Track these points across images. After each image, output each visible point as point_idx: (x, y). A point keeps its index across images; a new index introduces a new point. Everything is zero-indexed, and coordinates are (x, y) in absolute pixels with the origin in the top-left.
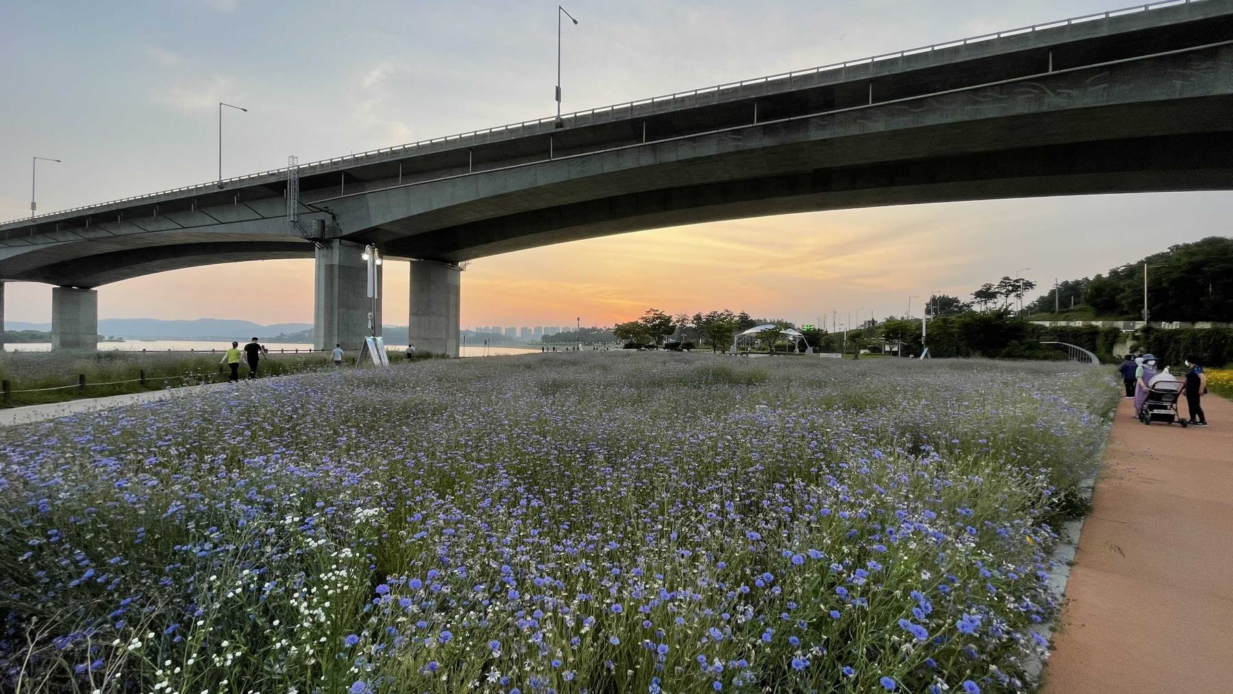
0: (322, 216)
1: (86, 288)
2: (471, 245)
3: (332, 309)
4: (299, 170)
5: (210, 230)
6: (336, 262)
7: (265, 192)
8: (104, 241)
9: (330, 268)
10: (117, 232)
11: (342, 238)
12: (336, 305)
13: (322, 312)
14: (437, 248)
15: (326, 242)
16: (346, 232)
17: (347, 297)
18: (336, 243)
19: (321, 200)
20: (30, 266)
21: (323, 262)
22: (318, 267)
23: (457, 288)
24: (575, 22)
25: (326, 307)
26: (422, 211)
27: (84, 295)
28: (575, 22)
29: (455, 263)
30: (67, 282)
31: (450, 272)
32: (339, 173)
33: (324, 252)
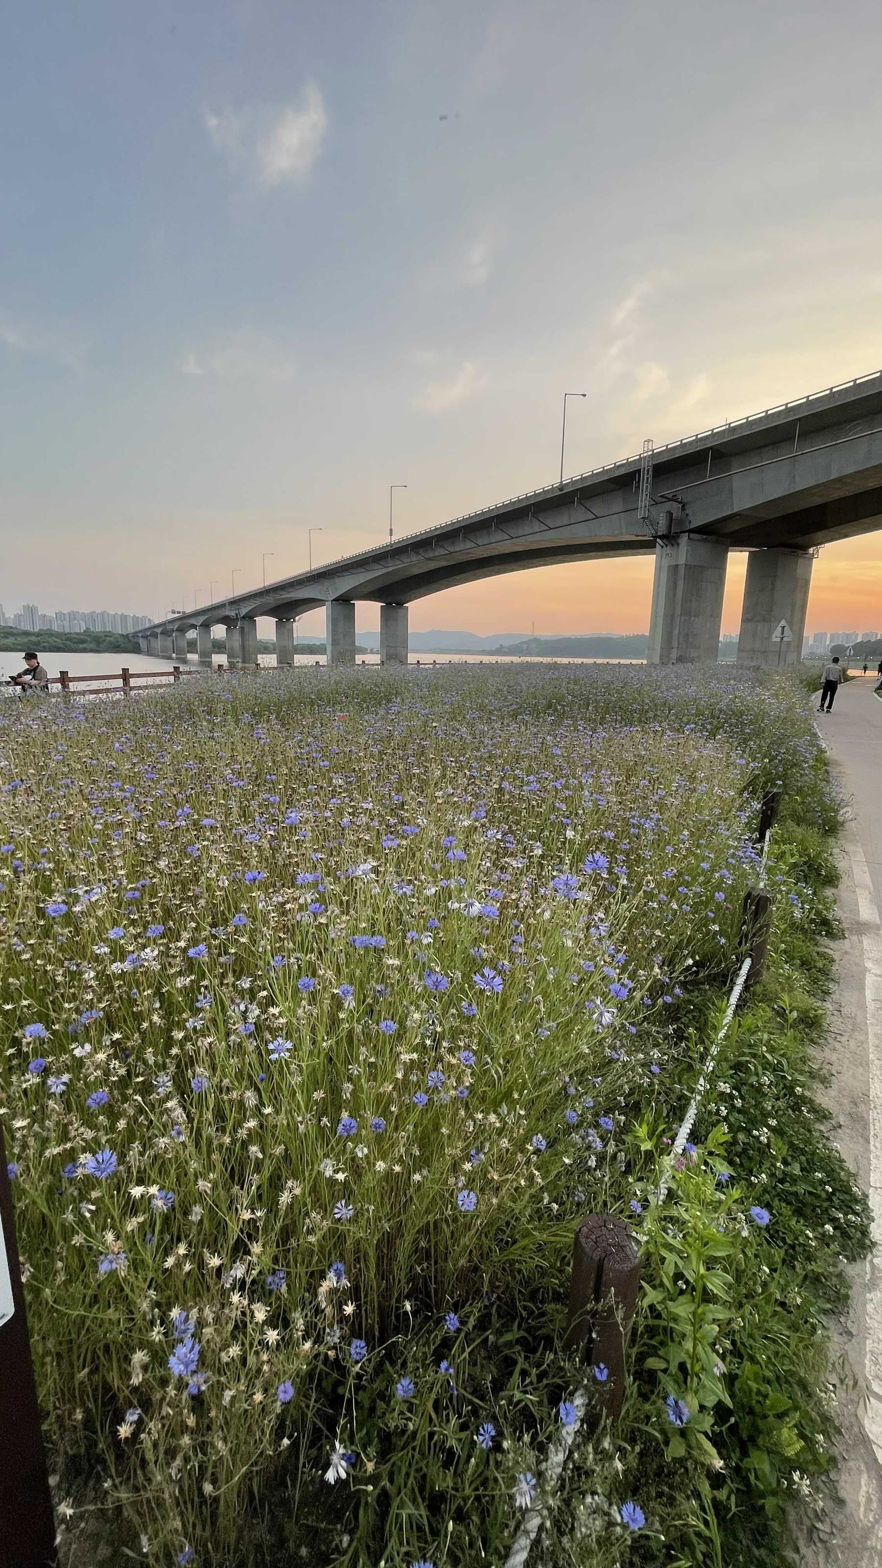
0: (668, 506)
1: (400, 604)
2: (499, 564)
3: (672, 617)
4: (654, 456)
5: (537, 537)
6: (682, 561)
7: (620, 483)
8: (416, 564)
9: (674, 569)
10: (451, 549)
11: (691, 531)
12: (678, 611)
13: (660, 621)
14: (786, 535)
15: (670, 538)
16: (698, 521)
17: (688, 598)
18: (684, 539)
19: (678, 488)
20: (371, 588)
21: (666, 563)
22: (659, 569)
23: (807, 582)
24: (584, 395)
25: (665, 615)
26: (812, 483)
27: (401, 612)
28: (584, 395)
29: (806, 548)
30: (389, 601)
31: (801, 561)
32: (706, 451)
33: (669, 550)
